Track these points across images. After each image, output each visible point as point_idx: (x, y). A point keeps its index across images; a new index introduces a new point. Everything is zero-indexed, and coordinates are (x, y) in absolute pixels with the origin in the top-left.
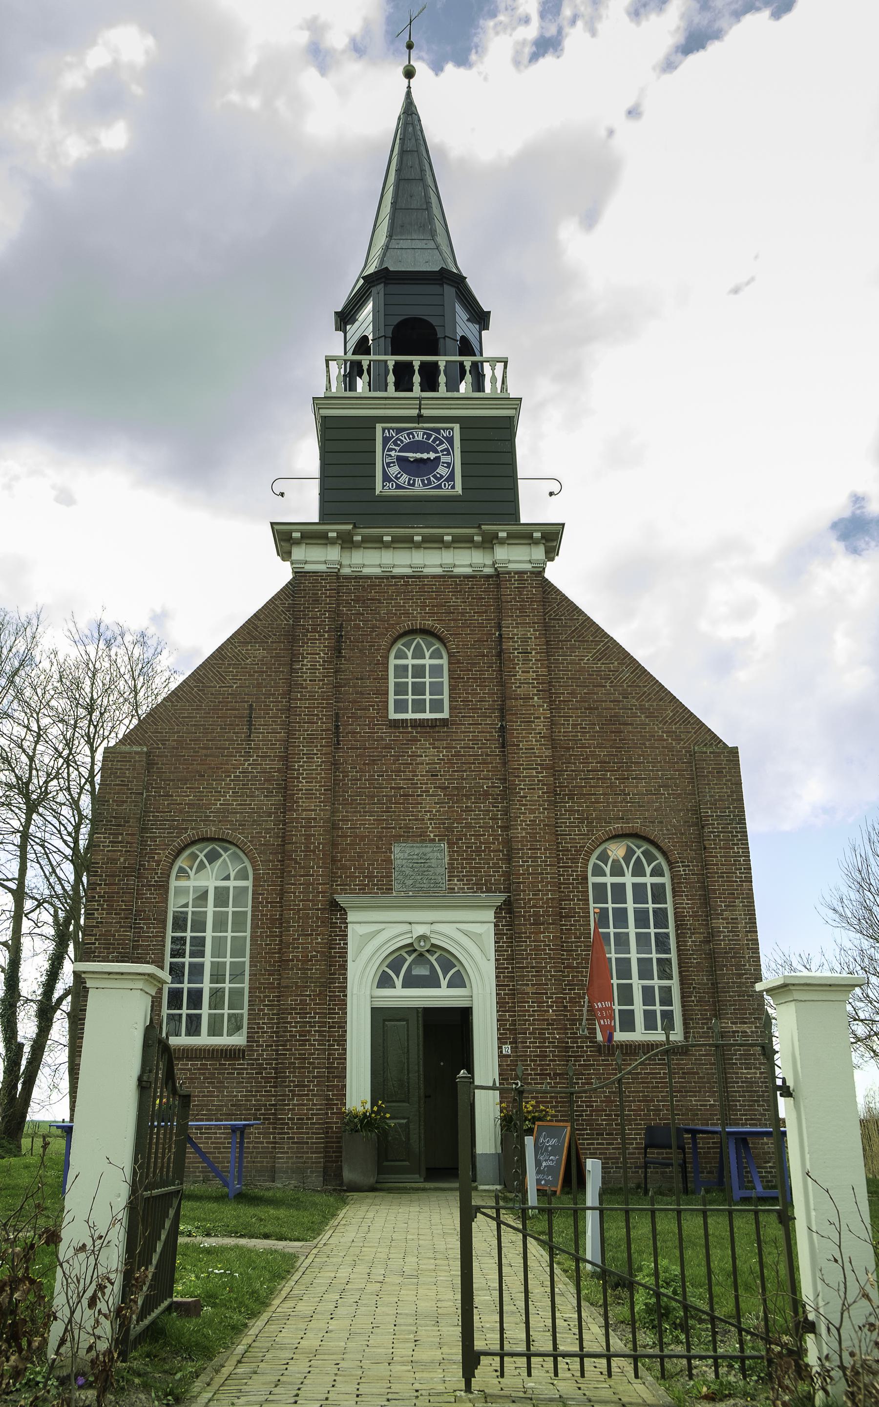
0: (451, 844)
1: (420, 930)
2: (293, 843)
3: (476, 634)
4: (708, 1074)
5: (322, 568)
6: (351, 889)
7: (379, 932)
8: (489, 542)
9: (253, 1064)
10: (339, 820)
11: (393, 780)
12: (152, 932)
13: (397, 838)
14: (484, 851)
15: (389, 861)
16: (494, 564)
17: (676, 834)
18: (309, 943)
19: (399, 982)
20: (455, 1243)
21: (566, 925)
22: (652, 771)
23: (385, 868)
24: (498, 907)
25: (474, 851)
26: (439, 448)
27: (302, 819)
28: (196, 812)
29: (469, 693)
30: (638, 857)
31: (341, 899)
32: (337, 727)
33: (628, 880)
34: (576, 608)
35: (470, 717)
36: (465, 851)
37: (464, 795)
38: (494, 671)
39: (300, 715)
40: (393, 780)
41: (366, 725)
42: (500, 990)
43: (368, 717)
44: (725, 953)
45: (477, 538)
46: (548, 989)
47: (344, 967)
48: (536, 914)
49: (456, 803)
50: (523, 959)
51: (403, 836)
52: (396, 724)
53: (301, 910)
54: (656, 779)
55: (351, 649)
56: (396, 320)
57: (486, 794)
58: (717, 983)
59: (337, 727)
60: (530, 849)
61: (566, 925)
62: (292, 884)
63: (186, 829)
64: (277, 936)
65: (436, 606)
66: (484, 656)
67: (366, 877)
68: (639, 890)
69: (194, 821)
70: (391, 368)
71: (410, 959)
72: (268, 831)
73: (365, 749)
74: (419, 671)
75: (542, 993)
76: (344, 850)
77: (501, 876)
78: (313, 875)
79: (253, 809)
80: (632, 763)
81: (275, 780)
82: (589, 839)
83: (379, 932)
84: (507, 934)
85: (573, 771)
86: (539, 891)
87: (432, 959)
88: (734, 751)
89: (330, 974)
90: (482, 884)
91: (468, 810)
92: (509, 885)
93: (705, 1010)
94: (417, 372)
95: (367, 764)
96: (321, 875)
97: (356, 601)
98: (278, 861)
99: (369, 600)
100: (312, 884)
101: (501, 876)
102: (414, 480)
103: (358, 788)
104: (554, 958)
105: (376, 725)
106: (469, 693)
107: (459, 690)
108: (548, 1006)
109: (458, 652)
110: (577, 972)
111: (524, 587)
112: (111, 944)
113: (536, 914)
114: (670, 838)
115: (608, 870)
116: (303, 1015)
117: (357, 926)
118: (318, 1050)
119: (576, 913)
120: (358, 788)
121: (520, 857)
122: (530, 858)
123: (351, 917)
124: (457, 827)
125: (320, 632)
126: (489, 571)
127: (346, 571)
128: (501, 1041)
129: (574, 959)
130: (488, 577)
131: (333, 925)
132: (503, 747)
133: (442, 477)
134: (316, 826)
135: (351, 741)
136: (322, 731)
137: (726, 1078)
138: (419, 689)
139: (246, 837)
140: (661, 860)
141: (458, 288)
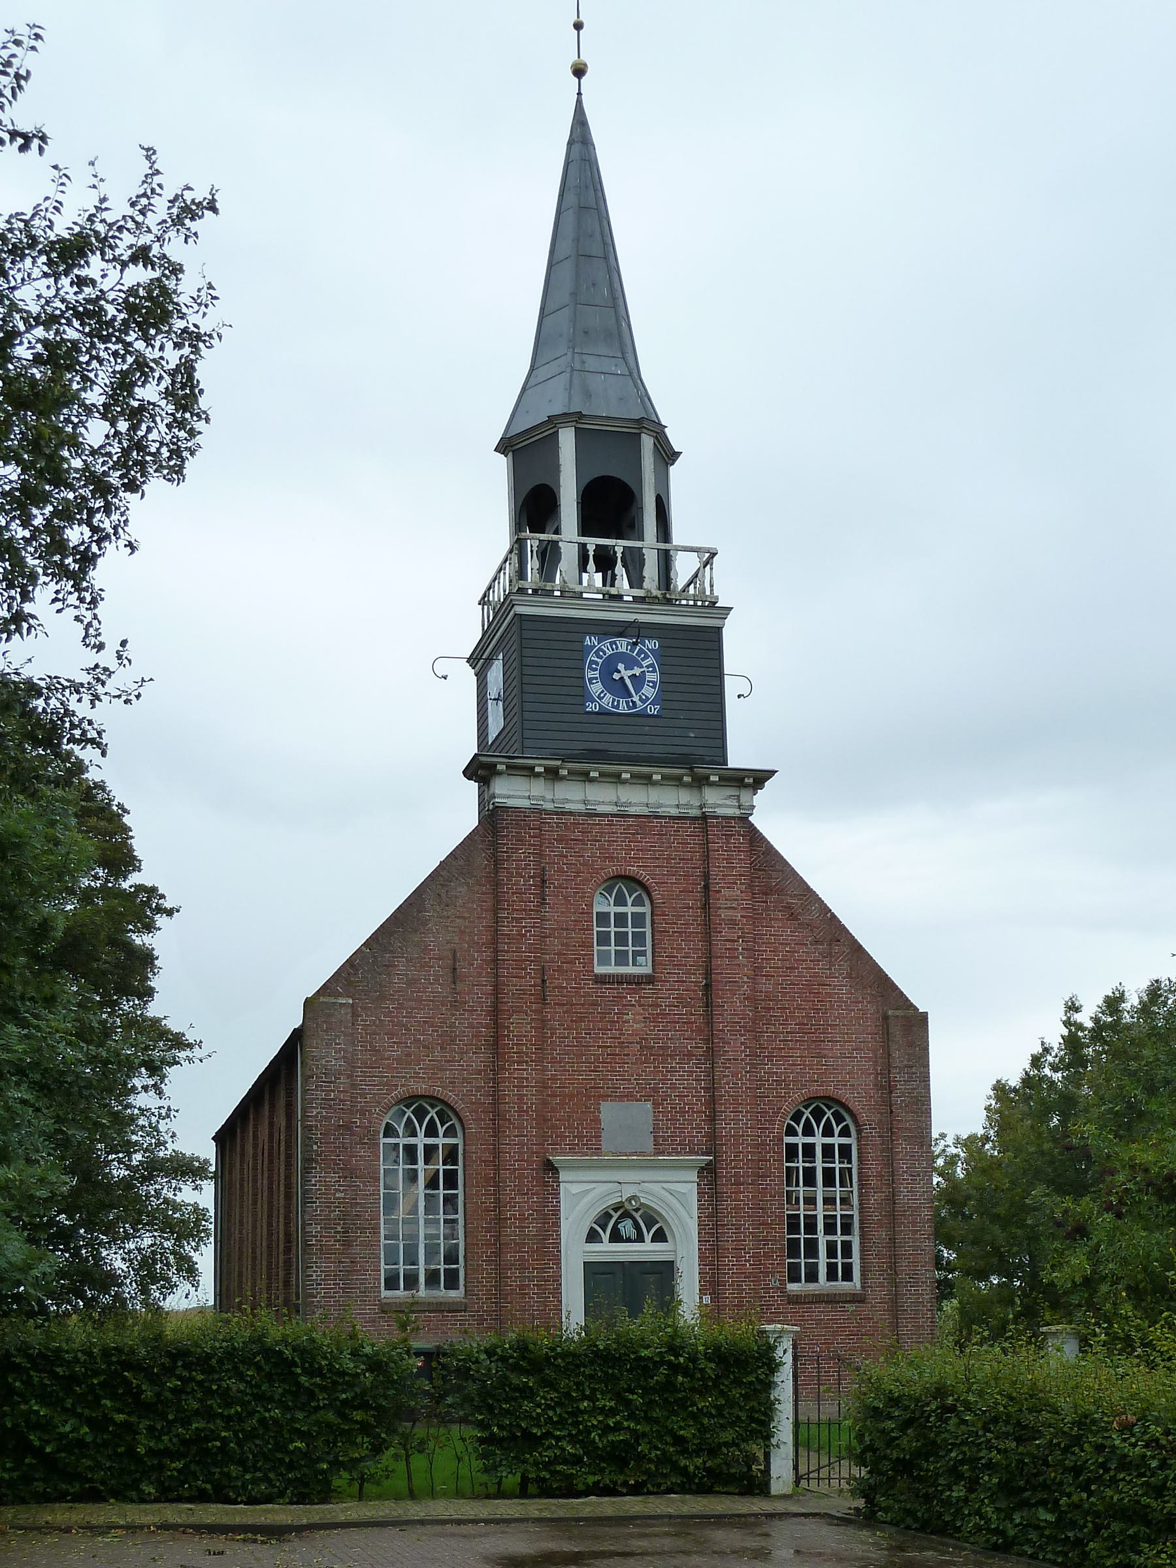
0: (656, 1105)
1: (628, 1192)
2: (506, 1103)
3: (681, 883)
4: (881, 1319)
5: (525, 803)
6: (561, 1149)
7: (587, 1192)
8: (700, 782)
9: (474, 1316)
10: (548, 1079)
11: (600, 1038)
12: (369, 1190)
13: (605, 1097)
14: (688, 1112)
15: (597, 1120)
16: (701, 807)
17: (866, 1097)
18: (525, 1202)
19: (606, 1237)
20: (356, 1535)
21: (762, 1184)
22: (847, 1034)
23: (594, 1128)
24: (702, 1168)
25: (678, 1112)
26: (645, 663)
27: (515, 1078)
28: (404, 1068)
29: (674, 949)
30: (828, 1118)
31: (556, 1159)
32: (544, 981)
33: (818, 1140)
34: (787, 863)
35: (675, 973)
36: (669, 1112)
37: (670, 1055)
38: (699, 925)
39: (508, 969)
40: (600, 1038)
41: (572, 980)
42: (557, 1206)
43: (575, 971)
44: (905, 1211)
45: (687, 779)
46: (747, 1245)
47: (557, 1224)
48: (736, 1175)
49: (662, 1063)
50: (724, 1217)
51: (610, 1096)
52: (602, 980)
53: (517, 1169)
54: (850, 1042)
55: (555, 896)
56: (587, 481)
57: (690, 1055)
58: (895, 1239)
59: (544, 981)
60: (732, 1112)
61: (762, 1184)
62: (507, 1144)
63: (397, 1085)
64: (491, 1195)
65: (642, 850)
66: (689, 908)
67: (576, 1137)
68: (828, 1150)
69: (403, 1077)
70: (591, 553)
71: (616, 1216)
72: (478, 1089)
73: (572, 1005)
74: (621, 919)
75: (741, 1249)
76: (553, 1110)
77: (703, 1137)
78: (527, 1136)
79: (463, 1066)
80: (828, 1025)
81: (483, 1036)
82: (786, 1101)
83: (587, 1192)
84: (708, 1193)
85: (773, 1032)
86: (741, 1152)
87: (637, 1216)
88: (924, 1017)
89: (546, 1231)
90: (686, 1145)
91: (673, 1071)
92: (713, 1144)
93: (883, 1263)
94: (619, 560)
95: (575, 1021)
96: (534, 1136)
97: (559, 841)
98: (490, 1120)
99: (572, 840)
100: (527, 1144)
101: (703, 1137)
102: (618, 701)
103: (565, 1046)
104: (752, 1217)
105: (583, 980)
106: (674, 949)
107: (665, 944)
108: (745, 1261)
109: (664, 903)
110: (771, 1228)
111: (732, 835)
112: (332, 1203)
113: (736, 1175)
114: (859, 1101)
115: (800, 1130)
116: (523, 1268)
117: (568, 1185)
118: (537, 1302)
119: (771, 1173)
120: (565, 1046)
121: (722, 1120)
122: (732, 1120)
123: (563, 1176)
124: (662, 1088)
125: (524, 877)
126: (695, 812)
127: (549, 806)
128: (702, 1292)
129: (768, 1217)
130: (695, 818)
131: (545, 1184)
132: (707, 1007)
133: (647, 698)
134: (527, 1086)
135: (558, 996)
136: (530, 986)
137: (897, 1323)
138: (621, 939)
139: (457, 1095)
140: (849, 1121)
141: (656, 437)
